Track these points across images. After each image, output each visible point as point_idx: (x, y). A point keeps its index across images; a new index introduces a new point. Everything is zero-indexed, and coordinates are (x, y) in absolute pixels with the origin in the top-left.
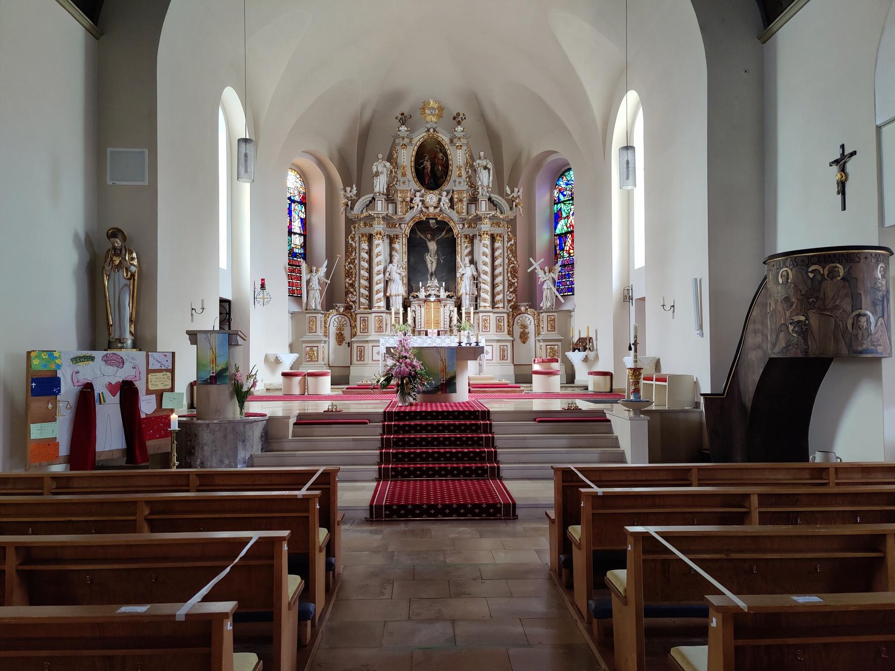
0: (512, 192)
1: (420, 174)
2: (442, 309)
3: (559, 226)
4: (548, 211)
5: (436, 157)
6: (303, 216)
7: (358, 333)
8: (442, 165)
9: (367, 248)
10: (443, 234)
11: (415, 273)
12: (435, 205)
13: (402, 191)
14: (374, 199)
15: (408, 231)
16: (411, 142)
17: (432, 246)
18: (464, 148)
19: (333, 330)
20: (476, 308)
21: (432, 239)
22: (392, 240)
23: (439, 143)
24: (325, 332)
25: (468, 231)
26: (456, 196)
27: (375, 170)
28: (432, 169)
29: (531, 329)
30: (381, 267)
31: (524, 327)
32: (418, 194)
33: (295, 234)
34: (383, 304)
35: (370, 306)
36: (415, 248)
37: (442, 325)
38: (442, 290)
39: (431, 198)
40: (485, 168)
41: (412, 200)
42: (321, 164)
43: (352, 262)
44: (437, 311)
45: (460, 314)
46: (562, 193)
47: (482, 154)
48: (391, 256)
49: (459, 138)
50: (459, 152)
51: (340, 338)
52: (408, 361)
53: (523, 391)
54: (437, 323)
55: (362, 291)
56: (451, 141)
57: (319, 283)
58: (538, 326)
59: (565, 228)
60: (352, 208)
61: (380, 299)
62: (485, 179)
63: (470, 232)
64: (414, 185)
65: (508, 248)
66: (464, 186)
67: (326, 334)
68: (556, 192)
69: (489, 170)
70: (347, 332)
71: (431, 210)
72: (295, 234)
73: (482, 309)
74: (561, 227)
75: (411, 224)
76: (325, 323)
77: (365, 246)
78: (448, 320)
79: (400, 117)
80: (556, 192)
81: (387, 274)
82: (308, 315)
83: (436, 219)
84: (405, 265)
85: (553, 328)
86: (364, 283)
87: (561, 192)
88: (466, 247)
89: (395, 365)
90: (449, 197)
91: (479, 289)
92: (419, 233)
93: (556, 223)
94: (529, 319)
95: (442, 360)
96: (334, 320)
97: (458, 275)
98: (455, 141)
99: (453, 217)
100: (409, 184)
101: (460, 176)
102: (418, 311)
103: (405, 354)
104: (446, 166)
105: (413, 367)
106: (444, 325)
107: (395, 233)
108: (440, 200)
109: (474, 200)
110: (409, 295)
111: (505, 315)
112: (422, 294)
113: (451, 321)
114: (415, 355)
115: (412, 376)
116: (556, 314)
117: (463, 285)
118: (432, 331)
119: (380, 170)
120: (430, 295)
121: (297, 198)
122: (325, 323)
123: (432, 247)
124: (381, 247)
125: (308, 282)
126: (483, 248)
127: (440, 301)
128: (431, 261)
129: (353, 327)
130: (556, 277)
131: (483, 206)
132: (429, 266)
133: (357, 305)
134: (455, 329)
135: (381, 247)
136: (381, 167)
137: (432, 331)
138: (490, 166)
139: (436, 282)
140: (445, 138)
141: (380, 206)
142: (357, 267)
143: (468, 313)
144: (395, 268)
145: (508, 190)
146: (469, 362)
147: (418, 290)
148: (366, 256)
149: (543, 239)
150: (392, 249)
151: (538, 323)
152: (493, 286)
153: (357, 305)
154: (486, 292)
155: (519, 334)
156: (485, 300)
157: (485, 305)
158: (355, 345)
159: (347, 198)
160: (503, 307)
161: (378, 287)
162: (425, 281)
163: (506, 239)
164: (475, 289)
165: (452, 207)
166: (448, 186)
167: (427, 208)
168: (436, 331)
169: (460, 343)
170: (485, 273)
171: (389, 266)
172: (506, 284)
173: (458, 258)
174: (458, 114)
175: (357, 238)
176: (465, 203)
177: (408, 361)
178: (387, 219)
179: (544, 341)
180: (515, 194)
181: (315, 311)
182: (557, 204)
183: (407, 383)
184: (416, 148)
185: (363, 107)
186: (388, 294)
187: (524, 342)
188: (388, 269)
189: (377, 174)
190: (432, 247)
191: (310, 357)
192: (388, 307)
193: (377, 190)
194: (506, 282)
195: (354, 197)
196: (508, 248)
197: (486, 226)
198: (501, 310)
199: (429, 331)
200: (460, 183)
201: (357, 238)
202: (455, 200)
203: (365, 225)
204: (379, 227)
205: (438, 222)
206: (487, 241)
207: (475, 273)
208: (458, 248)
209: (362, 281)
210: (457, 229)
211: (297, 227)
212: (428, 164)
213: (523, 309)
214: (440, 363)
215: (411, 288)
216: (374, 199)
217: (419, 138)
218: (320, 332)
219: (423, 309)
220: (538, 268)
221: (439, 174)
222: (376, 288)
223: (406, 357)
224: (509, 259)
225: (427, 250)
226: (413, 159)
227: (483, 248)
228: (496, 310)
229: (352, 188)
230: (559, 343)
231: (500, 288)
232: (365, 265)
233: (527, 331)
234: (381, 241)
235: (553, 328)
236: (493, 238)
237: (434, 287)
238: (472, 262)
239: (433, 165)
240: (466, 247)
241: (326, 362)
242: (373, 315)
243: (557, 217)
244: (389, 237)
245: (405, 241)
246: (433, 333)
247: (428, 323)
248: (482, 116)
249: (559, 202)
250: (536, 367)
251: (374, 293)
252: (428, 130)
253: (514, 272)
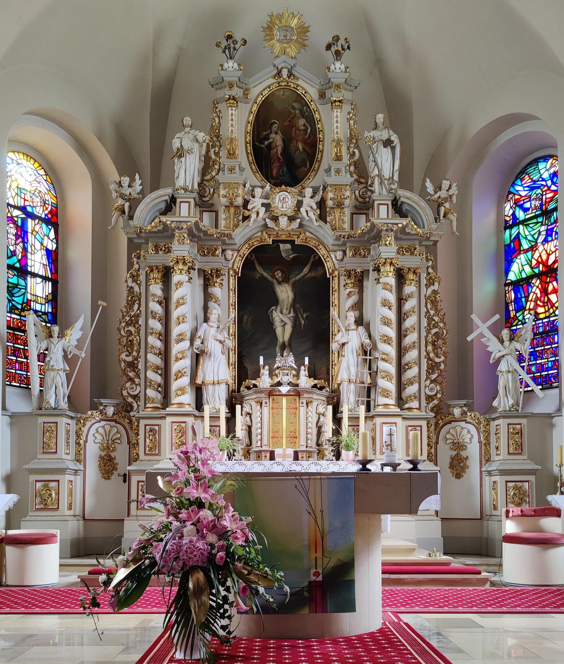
0: (438, 188)
1: (262, 158)
2: (303, 410)
3: (515, 267)
4: (493, 242)
5: (292, 125)
6: (52, 246)
7: (142, 456)
8: (304, 142)
9: (159, 293)
10: (306, 270)
11: (252, 344)
12: (290, 213)
13: (228, 185)
14: (173, 200)
15: (239, 265)
16: (246, 95)
17: (285, 293)
18: (347, 107)
19: (93, 450)
20: (368, 409)
21: (286, 280)
22: (208, 279)
23: (299, 99)
24: (78, 453)
25: (354, 263)
26: (330, 195)
27: (176, 144)
28: (284, 148)
29: (473, 450)
30: (185, 328)
31: (459, 446)
32: (258, 192)
33: (34, 275)
34: (188, 398)
35: (166, 401)
36: (253, 299)
37: (303, 441)
38: (304, 372)
39: (284, 200)
40: (388, 143)
41: (246, 203)
42: (82, 149)
43: (134, 321)
44: (293, 412)
45: (337, 421)
46: (521, 207)
47: (380, 117)
48: (206, 309)
49: (338, 86)
50: (337, 113)
51: (108, 465)
52: (206, 514)
53: (484, 581)
54: (293, 437)
55: (151, 375)
56: (322, 95)
57: (65, 357)
58: (485, 445)
59: (528, 269)
60: (131, 217)
61: (182, 390)
62: (385, 163)
63: (357, 265)
64: (252, 177)
65: (427, 298)
66: (346, 179)
67: (80, 458)
68: (508, 206)
69: (393, 149)
70: (121, 454)
71: (283, 221)
72: (34, 275)
73: (380, 409)
74: (520, 268)
75: (245, 251)
76: (78, 436)
77: (156, 289)
78: (315, 431)
79: (224, 43)
80: (508, 206)
81: (198, 342)
82: (41, 420)
83: (292, 242)
84: (233, 329)
85: (519, 449)
86: (155, 360)
87: (518, 204)
88: (349, 295)
89: (166, 528)
90: (318, 198)
91: (373, 374)
92: (259, 269)
93: (509, 263)
94: (469, 434)
95: (312, 512)
96: (95, 432)
97: (334, 346)
98: (328, 93)
99: (324, 237)
100: (240, 174)
101: (338, 158)
102: (257, 414)
103: (194, 493)
104: (312, 145)
105: (223, 534)
106: (306, 440)
107: (215, 266)
108: (299, 204)
109: (364, 206)
110: (240, 385)
111: (424, 423)
112: (265, 381)
113: (319, 433)
114: (231, 498)
115: (218, 566)
116: (524, 421)
117: (344, 364)
118: (285, 452)
119: (186, 147)
120: (279, 384)
121: (39, 211)
122: (78, 436)
123: (284, 302)
124: (186, 290)
125: (42, 357)
126: (380, 294)
127: (298, 394)
128: (283, 323)
129: (132, 445)
130: (525, 348)
131: (383, 214)
132: (279, 331)
133: (141, 403)
134: (328, 449)
135: (186, 290)
136: (189, 142)
137: (285, 452)
138: (394, 138)
139: (291, 360)
140: (309, 89)
141: (185, 211)
142: (142, 332)
143: (354, 419)
144: (213, 331)
145: (429, 185)
146: (383, 516)
147: (257, 375)
148: (158, 309)
149: (484, 288)
150: (208, 297)
151: (487, 438)
152: (401, 369)
153: (141, 403)
154: (387, 376)
155: (448, 460)
156: (385, 393)
157: (386, 402)
158: (134, 479)
159: (122, 196)
160: (419, 409)
161: (181, 365)
162: (270, 359)
163: (424, 282)
164: (366, 371)
165: (322, 217)
166: (317, 179)
167: (275, 219)
168: (291, 452)
169: (364, 463)
170: (387, 340)
171: (202, 325)
172: (424, 367)
173: (334, 312)
174: (336, 39)
175: (142, 278)
176: (347, 212)
177: (206, 514)
178: (196, 235)
179: (503, 472)
180: (443, 194)
181: (56, 412)
182: (511, 227)
183: (199, 591)
184: (255, 108)
185: (159, 35)
186: (199, 381)
187: (458, 476)
188: (200, 333)
189: (181, 153)
190: (284, 302)
191: (44, 501)
192: (199, 406)
193: (180, 183)
194: (424, 362)
195: (134, 195)
196: (427, 298)
197: (388, 250)
198: (416, 413)
199: (278, 451)
200: (338, 171)
201: (142, 278)
202: (330, 203)
203: (157, 248)
204: (182, 248)
205: (295, 248)
206: (391, 280)
207: (368, 341)
208: (334, 298)
209: (150, 357)
210: (332, 261)
211: (37, 262)
212: (277, 139)
213: (457, 412)
214: (306, 519)
215: (245, 371)
216: (173, 200)
217: (261, 87)
218: (65, 455)
219: (266, 410)
220: (488, 334)
221: (298, 158)
222: (175, 367)
223: (200, 505)
224: (430, 319)
225: (275, 301)
226: (250, 149)
227: (380, 294)
228: (406, 413)
229: (133, 180)
230: (532, 478)
231: (412, 373)
232: (156, 325)
233: (464, 454)
234: (184, 277)
235: (519, 449)
236: (401, 277)
237: (286, 370)
238: (359, 322)
239: (287, 142)
240: (349, 295)
241: (78, 510)
242: (169, 419)
243: (511, 251)
244: (202, 272)
245: (233, 283)
246: (284, 456)
247: (275, 436)
248: (378, 63)
249: (516, 222)
250: (510, 527)
251: (173, 377)
252: (279, 73)
253: (436, 342)
